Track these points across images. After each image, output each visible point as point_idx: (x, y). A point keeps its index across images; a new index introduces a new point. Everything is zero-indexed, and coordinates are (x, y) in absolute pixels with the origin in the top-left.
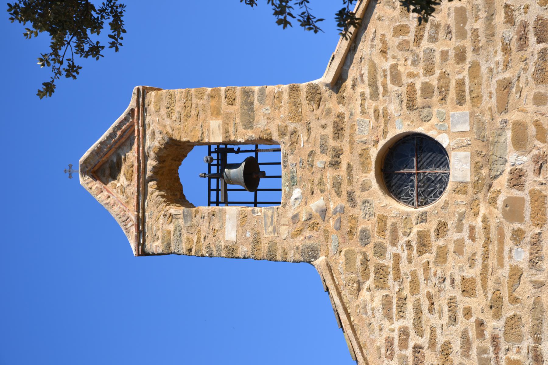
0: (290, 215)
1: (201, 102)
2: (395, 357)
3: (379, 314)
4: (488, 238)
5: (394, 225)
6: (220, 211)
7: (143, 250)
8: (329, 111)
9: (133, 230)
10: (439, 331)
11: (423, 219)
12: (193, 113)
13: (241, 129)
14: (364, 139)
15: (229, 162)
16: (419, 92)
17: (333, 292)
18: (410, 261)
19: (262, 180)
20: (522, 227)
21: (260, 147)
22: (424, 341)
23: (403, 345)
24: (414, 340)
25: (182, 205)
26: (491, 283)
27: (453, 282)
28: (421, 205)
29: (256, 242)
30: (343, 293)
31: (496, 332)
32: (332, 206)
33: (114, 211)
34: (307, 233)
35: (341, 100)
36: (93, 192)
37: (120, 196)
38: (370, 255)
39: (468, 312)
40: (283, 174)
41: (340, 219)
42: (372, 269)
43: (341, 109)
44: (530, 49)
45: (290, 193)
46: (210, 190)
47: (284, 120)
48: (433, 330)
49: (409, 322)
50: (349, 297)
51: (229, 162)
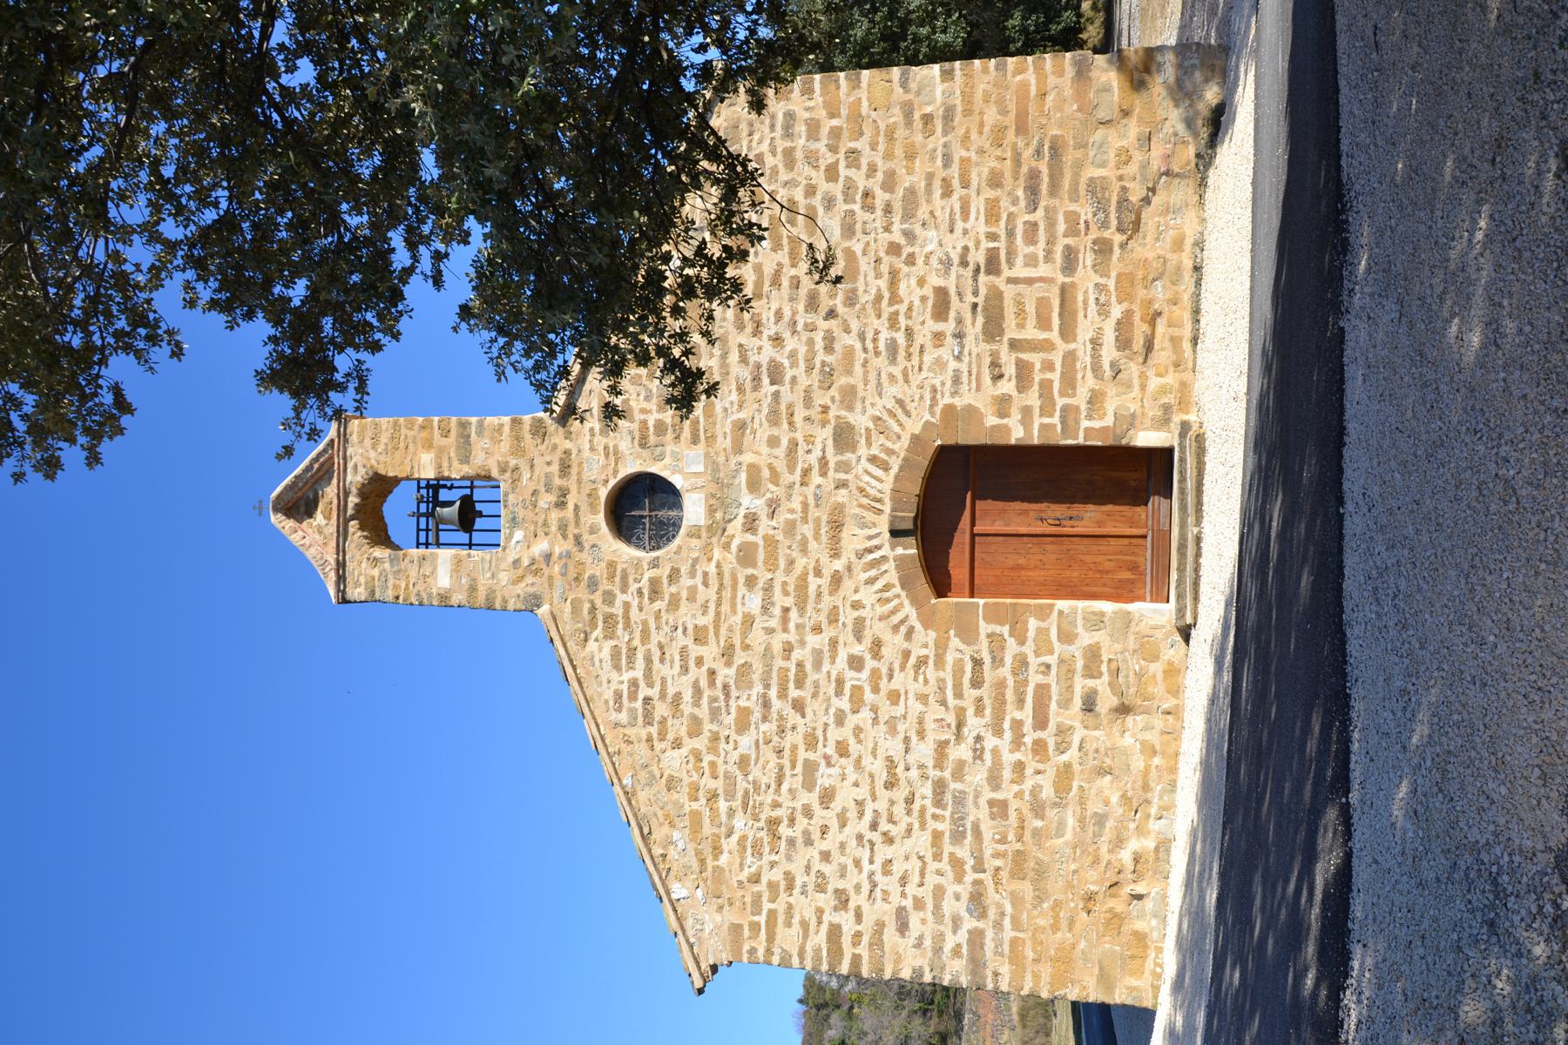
0: (510, 559)
1: (410, 433)
2: (624, 710)
3: (607, 665)
4: (722, 585)
5: (624, 572)
6: (431, 554)
7: (343, 598)
8: (555, 447)
9: (332, 575)
10: (669, 681)
11: (655, 564)
12: (402, 445)
13: (456, 463)
14: (593, 478)
15: (441, 499)
16: (652, 429)
17: (558, 643)
18: (641, 610)
19: (478, 520)
20: (755, 572)
21: (476, 483)
22: (654, 692)
23: (633, 696)
24: (644, 691)
25: (387, 547)
26: (723, 631)
27: (685, 630)
28: (653, 549)
29: (473, 589)
30: (568, 645)
31: (728, 680)
32: (557, 550)
33: (310, 554)
34: (530, 579)
35: (568, 435)
36: (286, 532)
37: (317, 536)
38: (598, 602)
39: (700, 661)
40: (503, 514)
41: (566, 564)
42: (600, 618)
43: (568, 445)
44: (763, 391)
45: (511, 535)
46: (419, 530)
47: (504, 455)
48: (664, 681)
49: (638, 673)
50: (575, 647)
51: (441, 499)
